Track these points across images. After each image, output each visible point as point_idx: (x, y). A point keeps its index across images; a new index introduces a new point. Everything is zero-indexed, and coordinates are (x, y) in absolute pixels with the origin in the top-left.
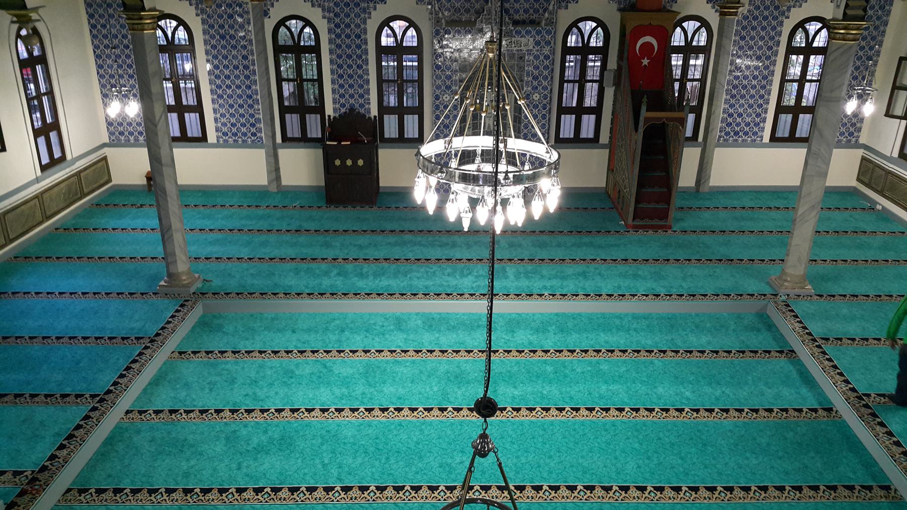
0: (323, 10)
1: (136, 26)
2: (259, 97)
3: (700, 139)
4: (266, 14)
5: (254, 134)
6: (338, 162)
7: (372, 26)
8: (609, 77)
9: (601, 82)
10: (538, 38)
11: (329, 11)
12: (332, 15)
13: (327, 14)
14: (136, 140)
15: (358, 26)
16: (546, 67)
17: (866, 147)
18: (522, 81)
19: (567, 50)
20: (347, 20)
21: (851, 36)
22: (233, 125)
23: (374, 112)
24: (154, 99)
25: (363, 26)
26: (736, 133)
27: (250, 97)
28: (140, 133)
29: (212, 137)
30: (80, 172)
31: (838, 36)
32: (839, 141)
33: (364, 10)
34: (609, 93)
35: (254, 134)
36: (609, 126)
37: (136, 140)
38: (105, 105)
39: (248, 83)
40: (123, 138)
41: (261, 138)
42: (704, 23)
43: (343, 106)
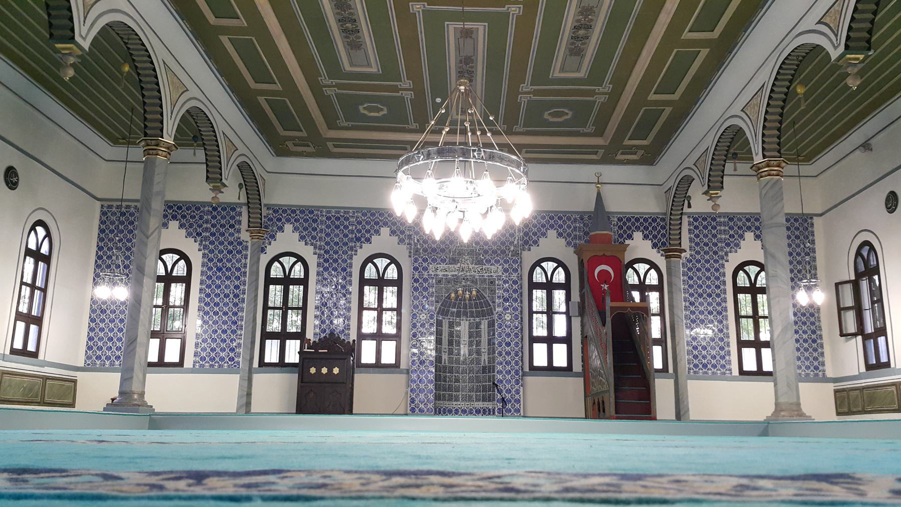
0: (315, 248)
1: (151, 152)
2: (243, 323)
3: (671, 370)
4: (263, 250)
5: (232, 359)
6: (313, 370)
7: (357, 262)
8: (574, 310)
9: (567, 313)
10: (506, 266)
11: (320, 249)
12: (322, 252)
13: (318, 251)
14: (112, 364)
15: (345, 261)
16: (515, 291)
17: (835, 380)
18: (494, 302)
19: (533, 286)
20: (335, 256)
21: (774, 172)
22: (213, 350)
23: (353, 336)
24: (152, 213)
25: (349, 261)
26: (705, 366)
27: (235, 323)
28: (118, 358)
29: (188, 363)
30: (48, 378)
31: (763, 174)
32: (807, 375)
33: (352, 249)
34: (576, 322)
35: (232, 359)
36: (580, 355)
37: (112, 364)
38: (95, 283)
39: (235, 310)
40: (98, 362)
41: (238, 363)
42: (653, 266)
43: (324, 331)
